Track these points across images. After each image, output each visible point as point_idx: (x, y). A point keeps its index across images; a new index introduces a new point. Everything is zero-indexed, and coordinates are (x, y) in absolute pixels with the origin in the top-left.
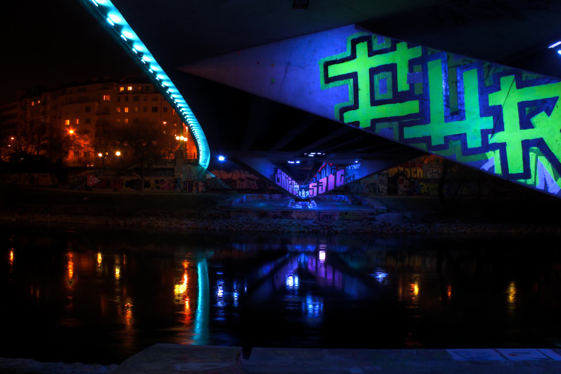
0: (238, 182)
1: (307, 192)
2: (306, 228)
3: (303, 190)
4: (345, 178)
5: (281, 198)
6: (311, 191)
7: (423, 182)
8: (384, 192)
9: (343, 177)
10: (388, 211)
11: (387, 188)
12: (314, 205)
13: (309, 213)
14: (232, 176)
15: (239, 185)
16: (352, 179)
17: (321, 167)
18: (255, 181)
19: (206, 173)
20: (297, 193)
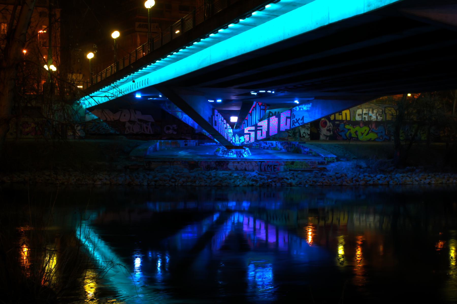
0: (128, 124)
1: (242, 138)
2: (253, 180)
3: (237, 135)
4: (292, 121)
5: (198, 144)
6: (247, 137)
7: (350, 125)
8: (306, 137)
9: (289, 120)
10: (338, 159)
11: (309, 133)
12: (249, 154)
13: (249, 163)
14: (120, 118)
15: (129, 128)
16: (300, 122)
17: (252, 107)
18: (150, 123)
19: (85, 114)
20: (231, 139)
